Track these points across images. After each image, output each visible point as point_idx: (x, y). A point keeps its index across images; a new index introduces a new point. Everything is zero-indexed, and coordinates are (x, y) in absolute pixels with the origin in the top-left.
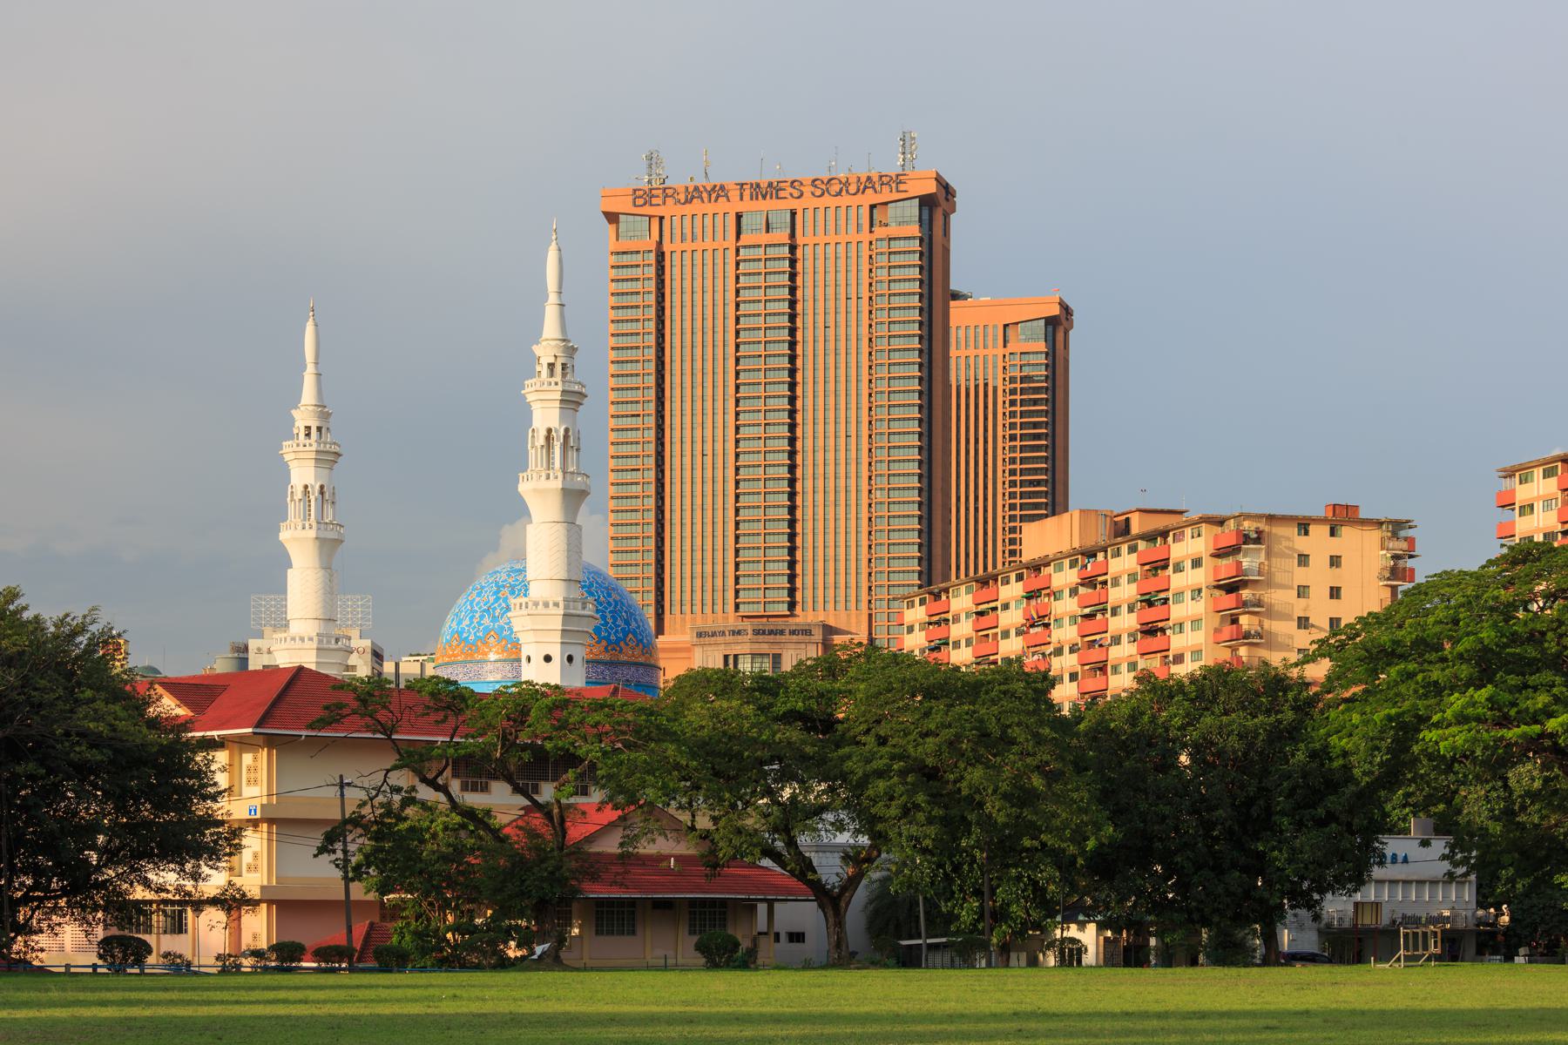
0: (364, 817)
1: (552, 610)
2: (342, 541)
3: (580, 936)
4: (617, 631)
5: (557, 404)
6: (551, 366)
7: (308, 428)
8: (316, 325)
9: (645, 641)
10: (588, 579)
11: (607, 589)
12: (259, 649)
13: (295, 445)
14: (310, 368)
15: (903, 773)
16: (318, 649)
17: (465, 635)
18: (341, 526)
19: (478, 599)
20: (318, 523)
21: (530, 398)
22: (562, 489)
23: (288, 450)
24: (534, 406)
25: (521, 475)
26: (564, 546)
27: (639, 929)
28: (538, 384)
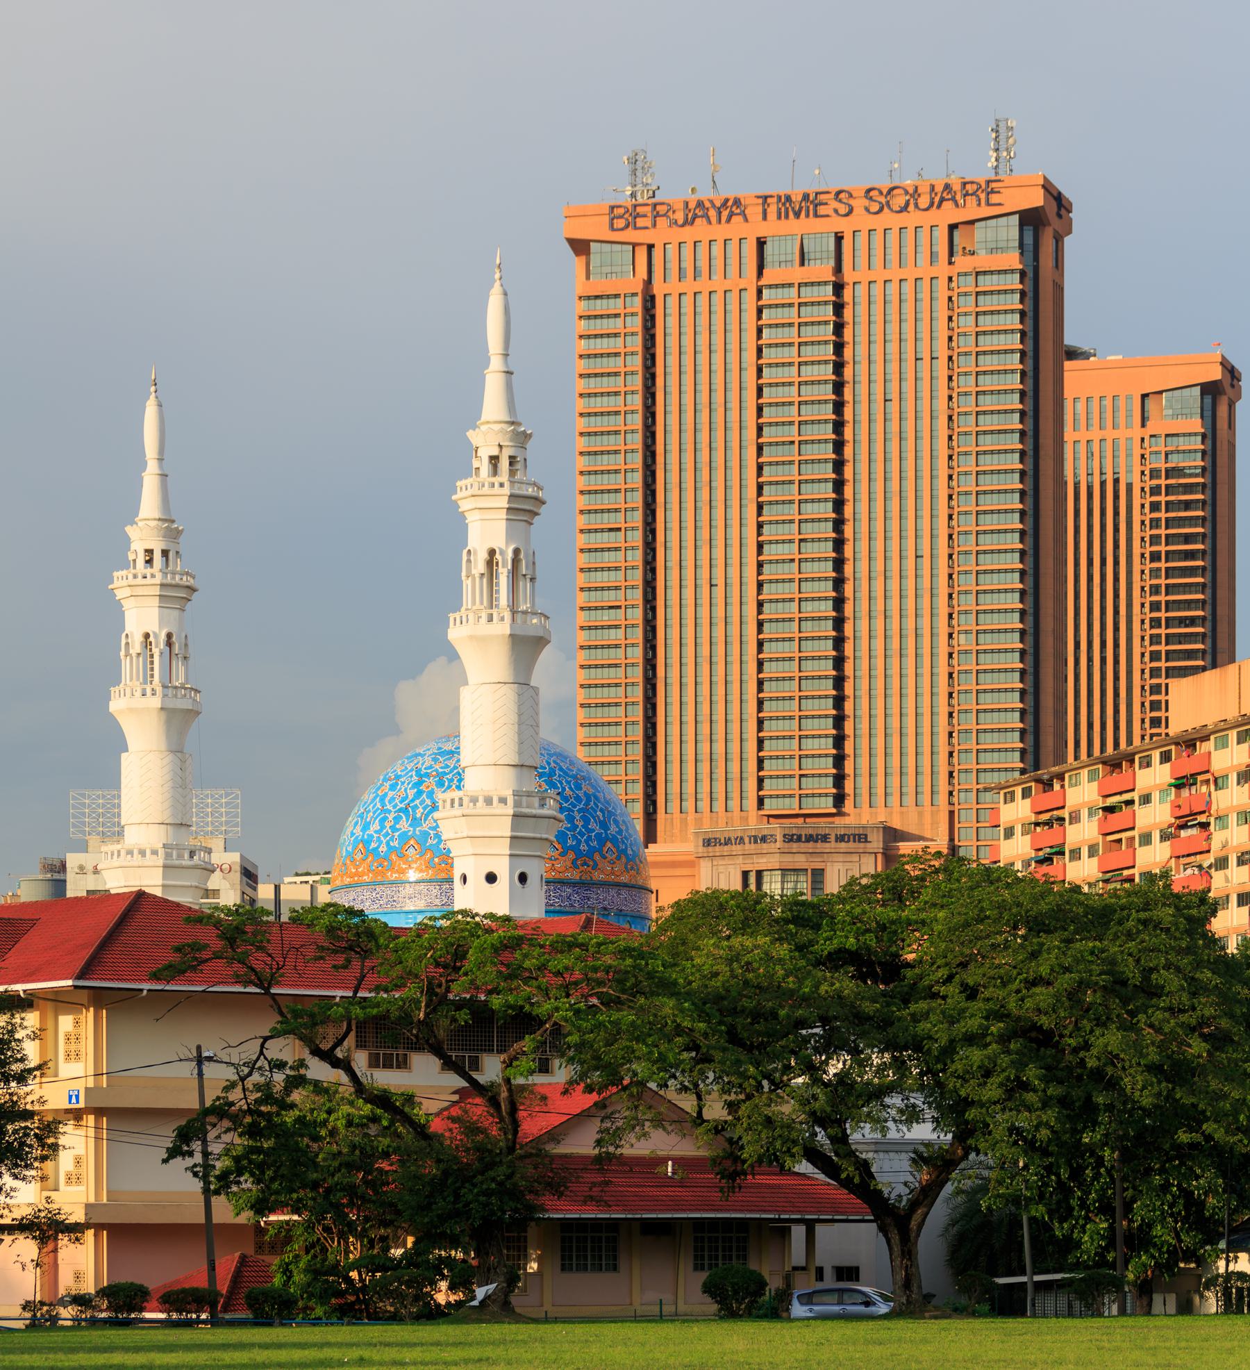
0: (232, 1104)
1: (497, 808)
2: (198, 713)
3: (539, 1273)
4: (589, 837)
5: (503, 515)
6: (494, 460)
7: (149, 552)
8: (160, 405)
9: (630, 852)
10: (549, 764)
11: (575, 777)
12: (81, 868)
13: (130, 576)
14: (152, 467)
15: (1004, 1039)
16: (165, 867)
17: (373, 845)
18: (197, 691)
19: (391, 794)
20: (164, 687)
21: (464, 506)
22: (511, 635)
23: (121, 583)
24: (470, 517)
25: (452, 616)
26: (513, 718)
27: (623, 1263)
28: (476, 486)
